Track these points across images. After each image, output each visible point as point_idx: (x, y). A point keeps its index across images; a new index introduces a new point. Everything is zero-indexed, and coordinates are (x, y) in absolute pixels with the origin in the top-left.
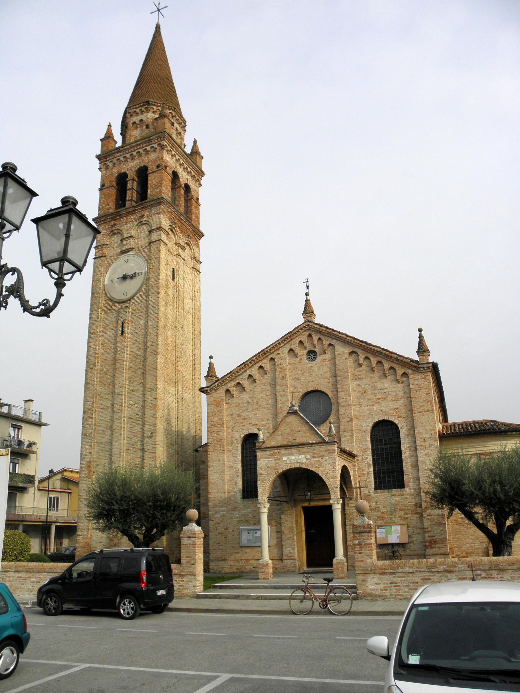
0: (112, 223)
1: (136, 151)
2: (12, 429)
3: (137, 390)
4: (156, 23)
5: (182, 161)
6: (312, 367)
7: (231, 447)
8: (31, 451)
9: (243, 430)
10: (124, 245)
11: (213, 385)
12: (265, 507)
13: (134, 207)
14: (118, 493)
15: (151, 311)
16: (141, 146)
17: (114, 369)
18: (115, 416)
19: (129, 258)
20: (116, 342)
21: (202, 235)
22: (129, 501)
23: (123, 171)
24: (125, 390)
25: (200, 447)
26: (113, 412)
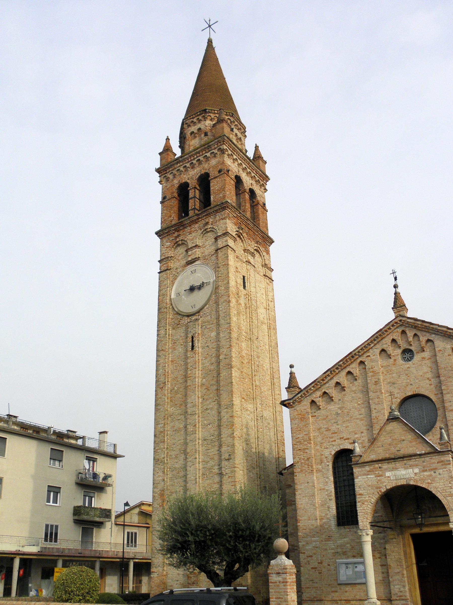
0: (176, 234)
1: (196, 160)
2: (87, 461)
3: (211, 409)
4: (208, 38)
5: (244, 166)
6: (409, 368)
7: (320, 467)
8: (107, 484)
9: (334, 446)
10: (190, 256)
11: (296, 397)
12: (368, 535)
13: (197, 215)
14: (192, 523)
15: (222, 321)
16: (201, 153)
17: (186, 388)
18: (188, 438)
19: (196, 268)
20: (186, 358)
21: (272, 242)
22: (206, 532)
23: (183, 181)
24: (198, 409)
25: (285, 469)
26: (186, 434)
